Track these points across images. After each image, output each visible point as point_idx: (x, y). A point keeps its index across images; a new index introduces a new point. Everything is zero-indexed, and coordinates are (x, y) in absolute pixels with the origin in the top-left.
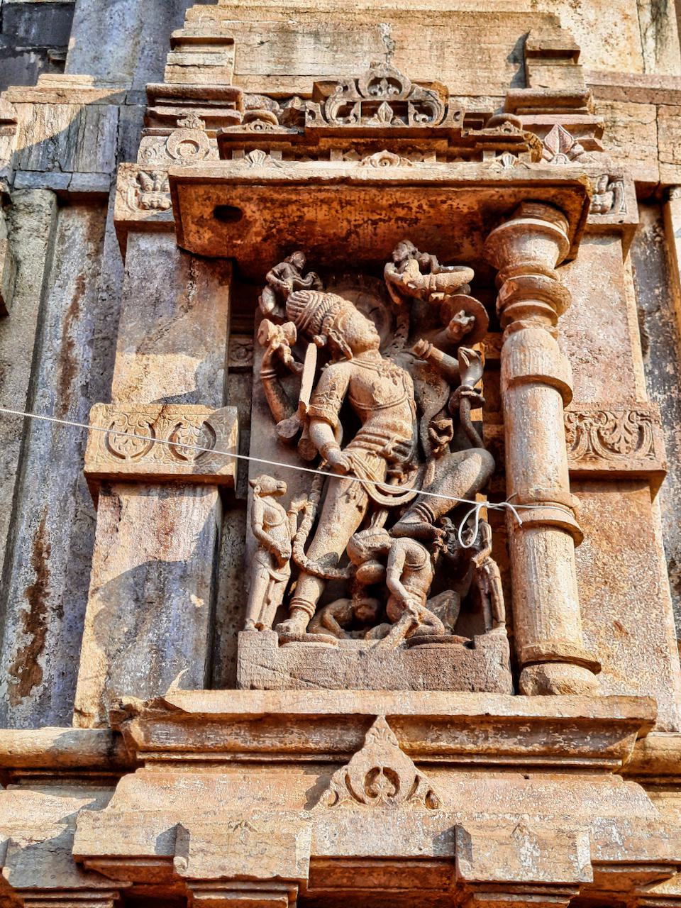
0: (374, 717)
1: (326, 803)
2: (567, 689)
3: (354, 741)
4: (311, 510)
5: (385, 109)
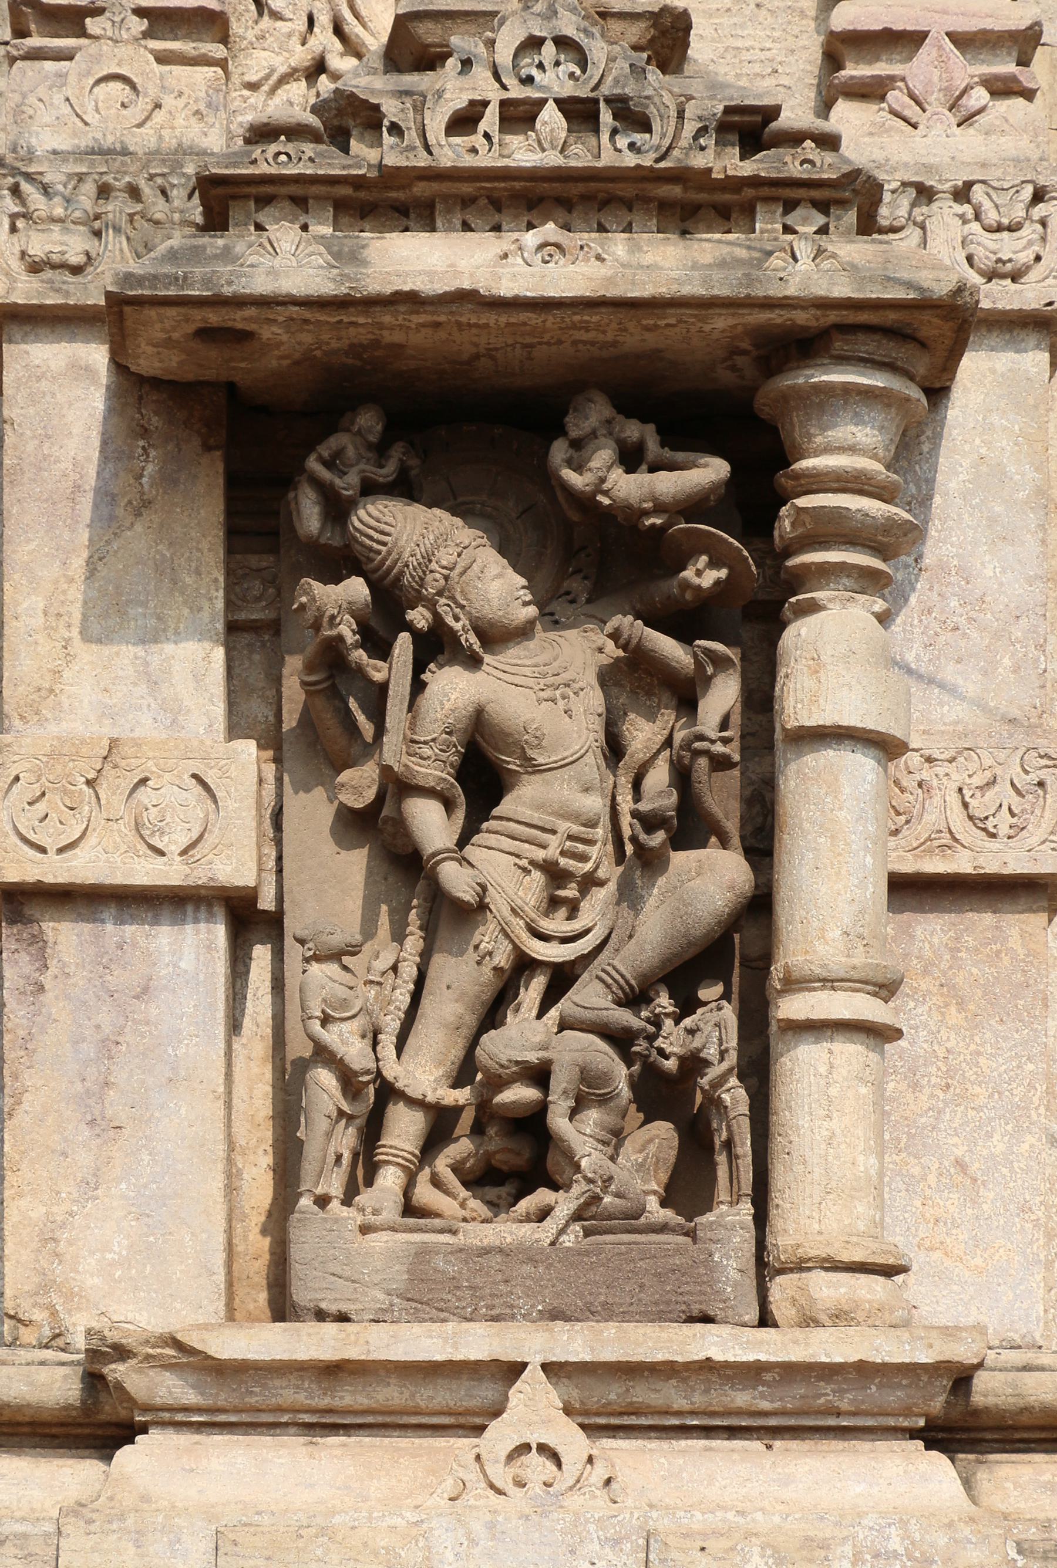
0: (524, 1365)
1: (446, 1496)
2: (841, 1317)
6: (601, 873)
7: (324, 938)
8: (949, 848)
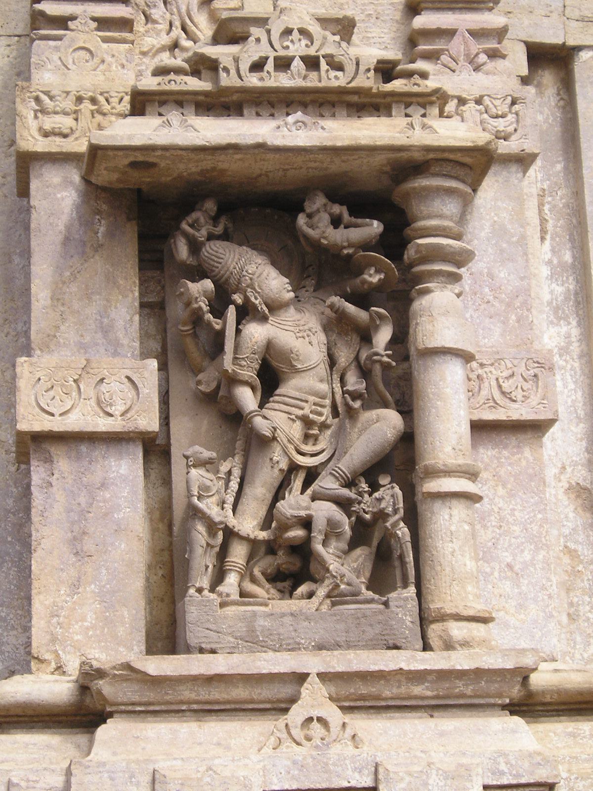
0: (308, 675)
2: (465, 644)
3: (290, 692)
4: (237, 472)
5: (297, 64)
6: (329, 422)
7: (199, 455)
8: (494, 407)
